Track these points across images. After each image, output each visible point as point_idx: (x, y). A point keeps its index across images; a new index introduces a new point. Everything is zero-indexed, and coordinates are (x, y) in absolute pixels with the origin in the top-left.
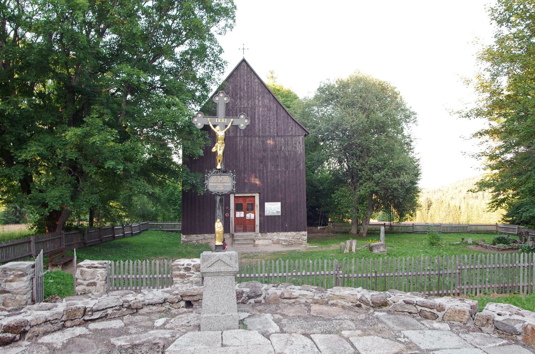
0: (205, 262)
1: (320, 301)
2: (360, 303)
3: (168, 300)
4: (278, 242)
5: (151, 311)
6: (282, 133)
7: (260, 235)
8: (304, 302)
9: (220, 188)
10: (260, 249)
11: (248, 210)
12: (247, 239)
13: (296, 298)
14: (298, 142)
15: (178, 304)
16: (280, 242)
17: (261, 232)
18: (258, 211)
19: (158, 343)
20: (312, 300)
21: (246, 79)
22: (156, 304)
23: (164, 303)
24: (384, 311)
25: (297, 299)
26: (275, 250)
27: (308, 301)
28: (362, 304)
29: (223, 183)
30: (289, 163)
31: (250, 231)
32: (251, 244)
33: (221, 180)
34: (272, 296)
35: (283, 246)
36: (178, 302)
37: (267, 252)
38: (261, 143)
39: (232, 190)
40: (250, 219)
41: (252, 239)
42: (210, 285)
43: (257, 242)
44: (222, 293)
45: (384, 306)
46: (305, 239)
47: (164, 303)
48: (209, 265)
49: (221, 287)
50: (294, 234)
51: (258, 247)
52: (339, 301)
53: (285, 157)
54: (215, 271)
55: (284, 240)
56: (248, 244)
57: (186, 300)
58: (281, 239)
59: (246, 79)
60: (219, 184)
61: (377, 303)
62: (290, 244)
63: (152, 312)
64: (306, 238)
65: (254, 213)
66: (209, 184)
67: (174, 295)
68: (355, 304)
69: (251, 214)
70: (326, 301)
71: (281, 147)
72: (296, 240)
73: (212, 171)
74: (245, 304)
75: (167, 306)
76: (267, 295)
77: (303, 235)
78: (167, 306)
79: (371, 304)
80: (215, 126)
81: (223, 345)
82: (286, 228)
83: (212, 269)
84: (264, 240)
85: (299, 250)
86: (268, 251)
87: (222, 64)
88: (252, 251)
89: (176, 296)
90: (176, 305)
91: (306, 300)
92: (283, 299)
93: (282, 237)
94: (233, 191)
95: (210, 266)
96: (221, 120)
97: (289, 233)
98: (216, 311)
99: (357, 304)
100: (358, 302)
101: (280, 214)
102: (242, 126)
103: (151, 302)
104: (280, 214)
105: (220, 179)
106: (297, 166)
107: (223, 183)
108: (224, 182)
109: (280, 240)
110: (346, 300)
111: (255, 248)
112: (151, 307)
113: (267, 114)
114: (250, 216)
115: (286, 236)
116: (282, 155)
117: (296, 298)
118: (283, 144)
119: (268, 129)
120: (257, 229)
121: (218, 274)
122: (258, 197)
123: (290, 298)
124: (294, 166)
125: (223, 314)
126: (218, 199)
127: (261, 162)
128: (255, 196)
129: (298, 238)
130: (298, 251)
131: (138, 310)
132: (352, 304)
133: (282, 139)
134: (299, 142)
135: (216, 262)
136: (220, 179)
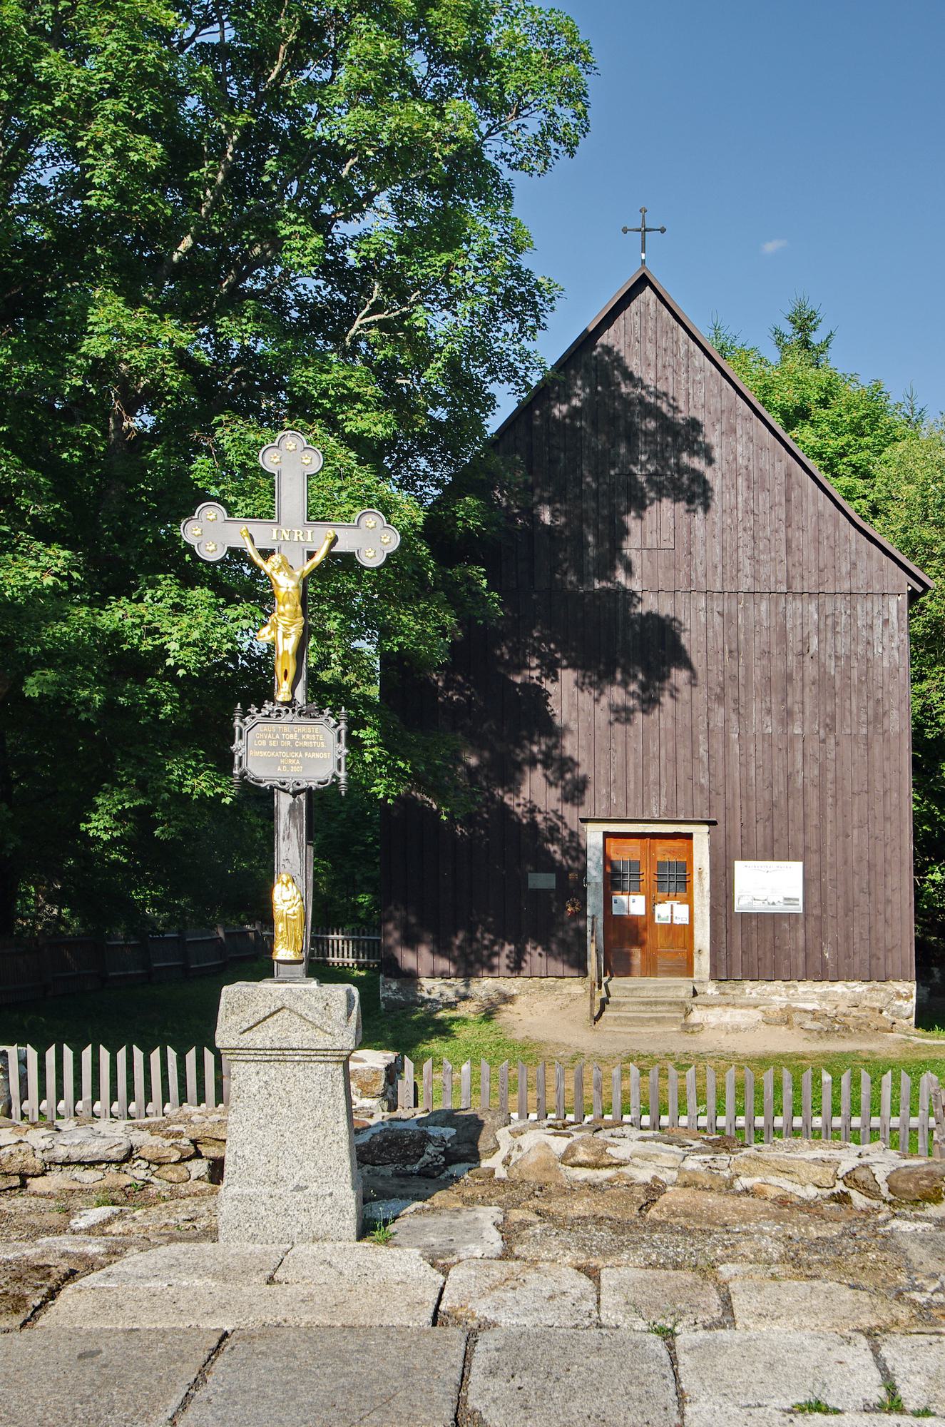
0: (233, 1013)
1: (704, 1179)
2: (845, 1189)
3: (142, 1154)
4: (787, 1018)
5: (76, 1186)
6: (810, 584)
7: (711, 989)
8: (649, 1180)
9: (289, 766)
10: (706, 1042)
11: (660, 886)
12: (656, 1003)
13: (619, 1165)
14: (878, 623)
15: (179, 1167)
16: (796, 1018)
17: (715, 976)
18: (707, 894)
19: (49, 1266)
20: (675, 1174)
21: (652, 357)
22: (100, 1162)
23: (125, 1160)
24: (928, 1220)
25: (622, 1169)
26: (769, 1048)
27: (662, 1177)
28: (854, 1194)
29: (301, 749)
30: (843, 707)
31: (671, 972)
32: (675, 1020)
33: (293, 742)
34: (532, 1158)
35: (805, 1035)
36: (181, 1161)
37: (734, 1054)
38: (717, 619)
39: (334, 776)
40: (672, 926)
41: (676, 1003)
42: (254, 1090)
43: (697, 1016)
44: (298, 1120)
45: (930, 1201)
46: (906, 1014)
47: (125, 1160)
48: (246, 1025)
49: (293, 1101)
50: (858, 989)
51: (703, 1037)
52: (773, 1180)
53: (823, 683)
54: (268, 1045)
55: (813, 1012)
56: (659, 1020)
57: (212, 1155)
58: (801, 1005)
59: (652, 357)
60: (285, 754)
61: (905, 1191)
62: (834, 1025)
63: (81, 1190)
64: (910, 1006)
65: (689, 901)
66: (251, 753)
67: (167, 1137)
68: (828, 1192)
69: (675, 903)
70: (724, 1179)
71: (805, 641)
72: (870, 1013)
73: (260, 707)
74: (433, 1177)
75: (138, 1172)
76: (514, 1153)
77: (899, 995)
78: (141, 1174)
79: (884, 1188)
80: (266, 554)
81: (271, 1280)
82: (824, 963)
83: (259, 1038)
84: (730, 1009)
85: (871, 1052)
86: (739, 1051)
87: (533, 295)
88: (674, 1049)
89: (173, 1141)
90: (174, 1171)
91: (654, 1173)
92: (573, 1166)
93: (805, 1000)
94: (338, 779)
95: (250, 1029)
96: (291, 533)
97: (839, 987)
98: (273, 1179)
99: (835, 1190)
100: (840, 1187)
101: (799, 908)
102: (372, 557)
103: (76, 1154)
104: (799, 908)
105: (291, 737)
106: (877, 719)
107: (301, 749)
108: (307, 749)
109: (795, 1010)
110: (796, 1179)
111: (688, 1037)
112: (78, 1172)
113: (746, 501)
114: (670, 912)
115: (824, 997)
116: (811, 670)
117: (619, 1165)
118: (812, 628)
119: (747, 566)
120: (702, 964)
121: (279, 1054)
122: (706, 839)
123: (596, 1166)
124: (864, 718)
125: (298, 1188)
126: (284, 802)
127: (720, 699)
128: (689, 836)
129: (877, 1005)
130: (866, 1056)
131: (29, 1181)
132: (819, 1191)
133: (812, 608)
134: (886, 622)
135: (271, 1015)
136: (291, 737)
